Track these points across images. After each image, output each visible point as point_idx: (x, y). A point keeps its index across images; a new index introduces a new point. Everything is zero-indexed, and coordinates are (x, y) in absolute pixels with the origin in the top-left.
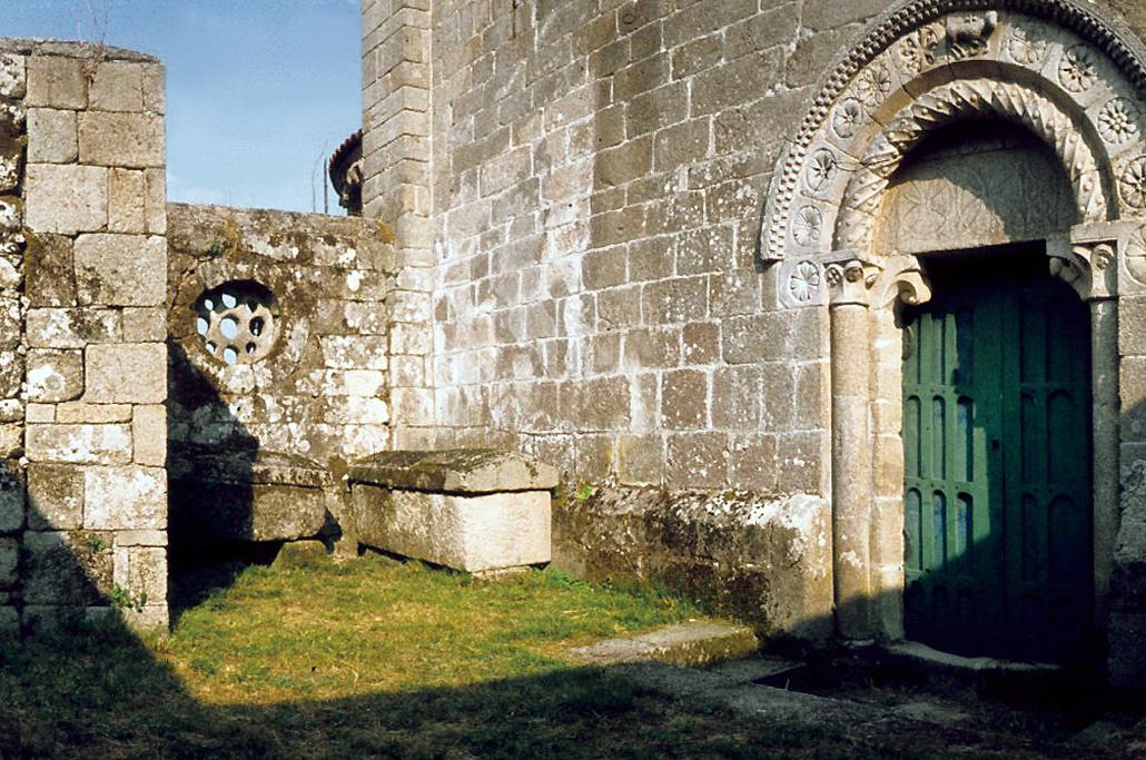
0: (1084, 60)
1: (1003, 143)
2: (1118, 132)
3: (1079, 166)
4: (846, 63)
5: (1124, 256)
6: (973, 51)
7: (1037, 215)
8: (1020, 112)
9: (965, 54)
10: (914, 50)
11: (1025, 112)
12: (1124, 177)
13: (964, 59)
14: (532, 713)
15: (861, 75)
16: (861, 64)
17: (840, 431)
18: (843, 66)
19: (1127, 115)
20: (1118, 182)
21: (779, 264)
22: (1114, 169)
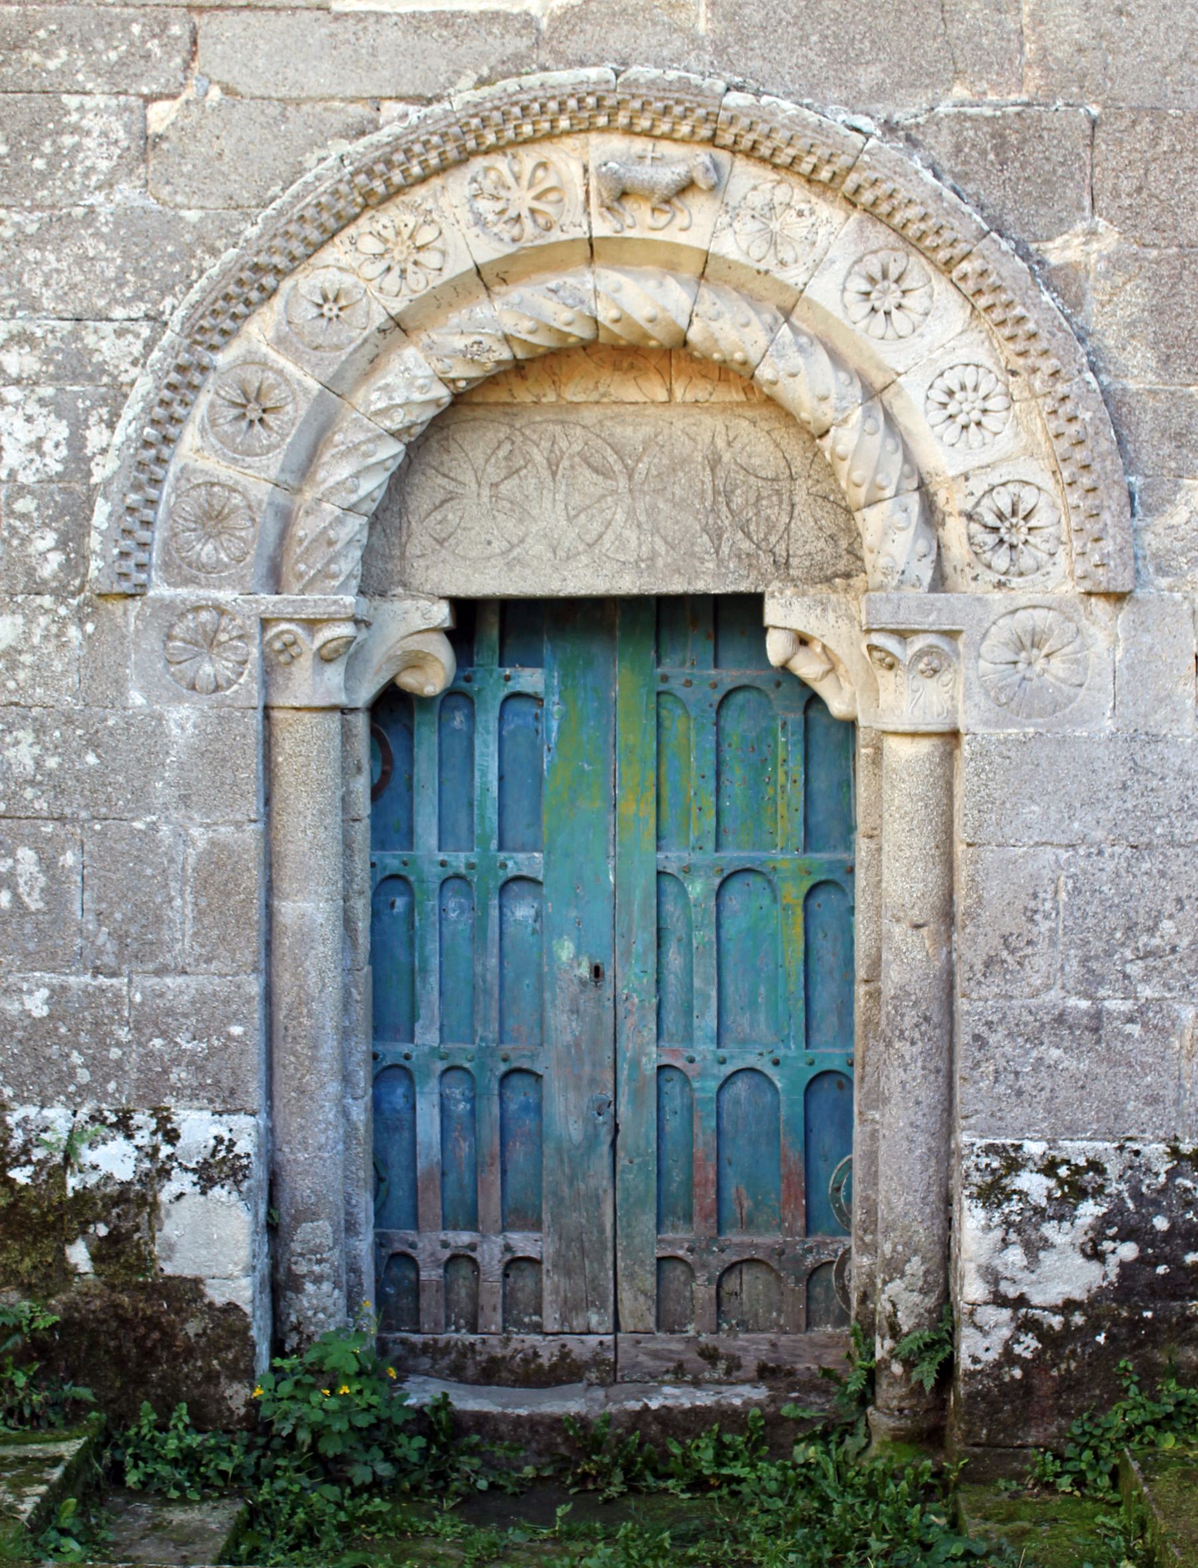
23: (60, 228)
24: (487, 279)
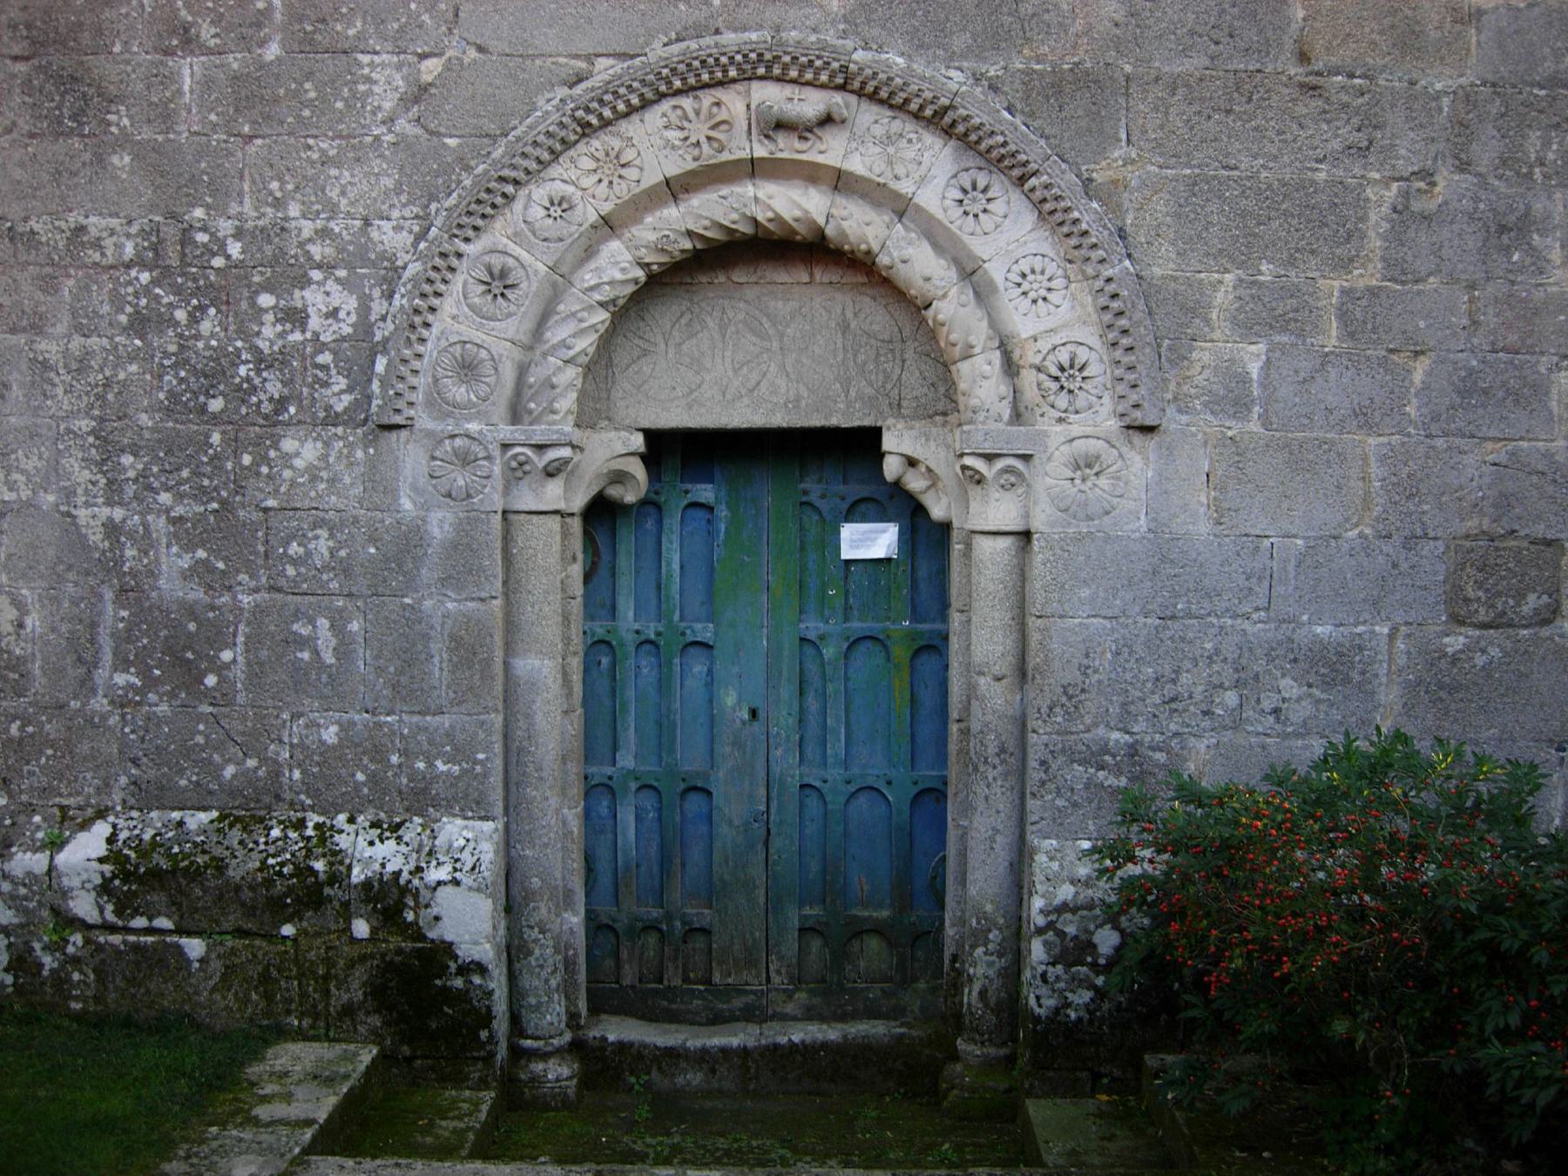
1: (811, 275)
7: (869, 391)
9: (787, 147)
10: (686, 124)
16: (586, 130)
17: (527, 716)
23: (356, 151)
24: (675, 189)
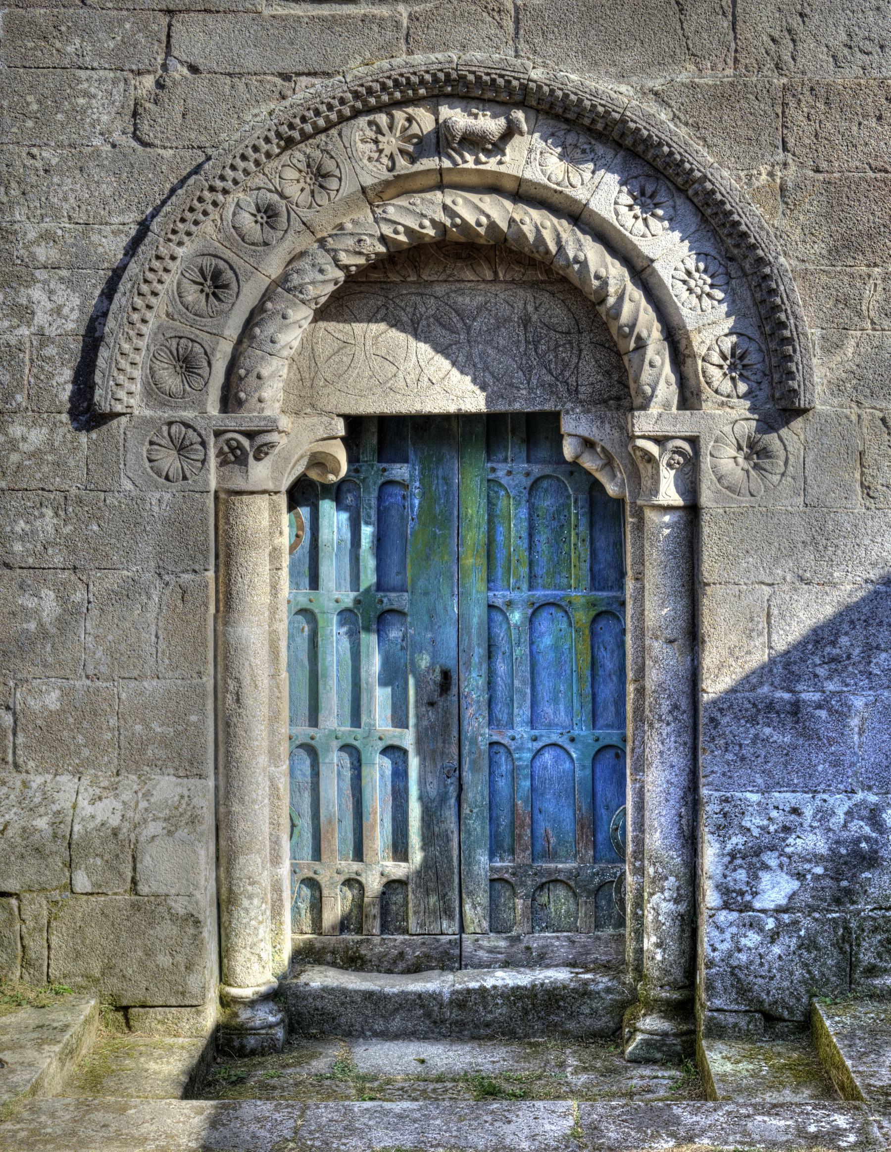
0: (652, 197)
2: (699, 297)
3: (644, 334)
4: (267, 140)
5: (709, 458)
6: (482, 158)
7: (548, 378)
8: (553, 248)
11: (560, 247)
12: (707, 355)
13: (465, 166)
14: (751, 925)
15: (285, 157)
18: (263, 143)
19: (712, 277)
20: (700, 362)
21: (124, 420)
22: (695, 344)
